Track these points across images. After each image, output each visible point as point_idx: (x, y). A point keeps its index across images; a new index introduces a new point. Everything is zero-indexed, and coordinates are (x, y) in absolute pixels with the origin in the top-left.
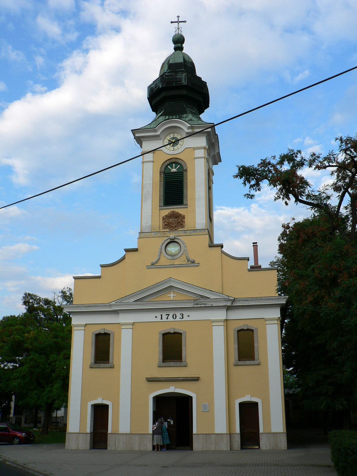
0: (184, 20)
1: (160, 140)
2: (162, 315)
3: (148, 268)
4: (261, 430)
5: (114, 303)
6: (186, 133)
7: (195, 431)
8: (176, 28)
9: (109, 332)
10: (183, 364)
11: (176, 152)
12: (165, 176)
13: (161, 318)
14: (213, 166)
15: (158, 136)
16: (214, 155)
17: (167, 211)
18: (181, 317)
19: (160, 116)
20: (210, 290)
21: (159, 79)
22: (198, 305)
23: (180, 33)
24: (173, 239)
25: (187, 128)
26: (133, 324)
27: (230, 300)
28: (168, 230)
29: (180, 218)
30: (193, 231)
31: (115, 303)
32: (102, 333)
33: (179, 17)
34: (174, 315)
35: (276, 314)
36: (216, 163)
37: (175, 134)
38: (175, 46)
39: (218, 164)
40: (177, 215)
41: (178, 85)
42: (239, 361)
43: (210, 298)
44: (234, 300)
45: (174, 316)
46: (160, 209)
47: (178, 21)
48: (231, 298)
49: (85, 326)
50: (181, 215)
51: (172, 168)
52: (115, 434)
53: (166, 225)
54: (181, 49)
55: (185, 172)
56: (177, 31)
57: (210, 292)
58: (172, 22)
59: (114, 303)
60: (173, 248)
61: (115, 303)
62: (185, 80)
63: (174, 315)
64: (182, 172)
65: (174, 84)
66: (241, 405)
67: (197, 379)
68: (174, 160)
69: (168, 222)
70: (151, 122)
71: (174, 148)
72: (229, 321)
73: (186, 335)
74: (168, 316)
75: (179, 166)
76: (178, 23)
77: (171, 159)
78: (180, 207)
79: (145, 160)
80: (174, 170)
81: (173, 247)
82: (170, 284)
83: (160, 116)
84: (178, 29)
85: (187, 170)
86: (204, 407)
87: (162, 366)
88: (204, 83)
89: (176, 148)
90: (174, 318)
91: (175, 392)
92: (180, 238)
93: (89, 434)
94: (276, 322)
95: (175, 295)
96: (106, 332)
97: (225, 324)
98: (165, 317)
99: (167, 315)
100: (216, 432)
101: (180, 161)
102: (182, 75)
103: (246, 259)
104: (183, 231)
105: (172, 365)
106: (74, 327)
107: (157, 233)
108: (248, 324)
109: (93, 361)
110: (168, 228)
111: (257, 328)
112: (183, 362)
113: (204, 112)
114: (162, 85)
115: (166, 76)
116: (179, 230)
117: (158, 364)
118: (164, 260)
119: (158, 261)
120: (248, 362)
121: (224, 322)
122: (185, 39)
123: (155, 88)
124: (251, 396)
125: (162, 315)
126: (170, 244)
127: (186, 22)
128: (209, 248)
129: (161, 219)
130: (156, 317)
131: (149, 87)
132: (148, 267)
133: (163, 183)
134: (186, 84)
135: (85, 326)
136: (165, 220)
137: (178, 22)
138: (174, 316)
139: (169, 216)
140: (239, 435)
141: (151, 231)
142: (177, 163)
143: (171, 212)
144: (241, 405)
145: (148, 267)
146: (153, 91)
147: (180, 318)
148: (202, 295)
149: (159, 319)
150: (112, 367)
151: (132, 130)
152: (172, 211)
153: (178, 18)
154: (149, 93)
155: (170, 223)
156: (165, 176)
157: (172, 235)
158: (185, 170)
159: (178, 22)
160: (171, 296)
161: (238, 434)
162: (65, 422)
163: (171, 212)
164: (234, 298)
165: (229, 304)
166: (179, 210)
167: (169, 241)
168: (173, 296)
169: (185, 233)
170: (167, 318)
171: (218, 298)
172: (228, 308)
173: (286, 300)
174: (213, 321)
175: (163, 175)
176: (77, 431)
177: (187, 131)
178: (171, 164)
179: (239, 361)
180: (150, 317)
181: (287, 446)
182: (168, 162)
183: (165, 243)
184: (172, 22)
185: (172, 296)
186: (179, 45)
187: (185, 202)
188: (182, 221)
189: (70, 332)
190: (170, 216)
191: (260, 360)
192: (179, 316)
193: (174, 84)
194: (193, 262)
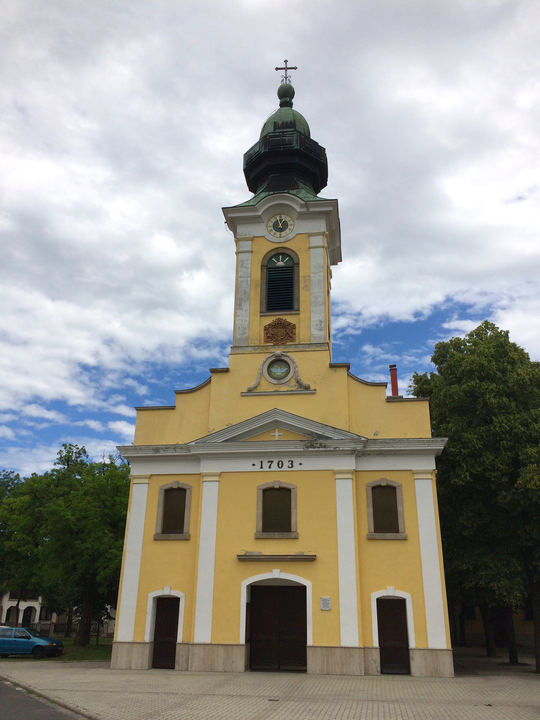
0: (293, 67)
1: (263, 223)
2: (262, 462)
3: (242, 396)
4: (412, 644)
5: (193, 443)
6: (297, 214)
7: (310, 642)
8: (283, 77)
9: (185, 487)
10: (293, 535)
11: (282, 240)
12: (269, 271)
13: (260, 467)
14: (331, 266)
15: (259, 217)
16: (333, 249)
17: (269, 320)
18: (290, 466)
19: (261, 192)
20: (332, 427)
21: (261, 141)
22: (315, 448)
23: (288, 83)
24: (279, 356)
25: (300, 205)
26: (220, 475)
27: (362, 442)
28: (272, 344)
29: (289, 328)
30: (307, 345)
31: (195, 443)
32: (174, 487)
33: (287, 61)
34: (280, 463)
35: (431, 465)
36: (334, 263)
37: (282, 215)
38: (281, 102)
39: (337, 265)
40: (285, 324)
41: (287, 149)
42: (374, 533)
43: (332, 438)
44: (367, 441)
45: (280, 464)
46: (261, 316)
47: (286, 67)
48: (363, 439)
49: (149, 478)
50: (290, 323)
51: (279, 261)
52: (187, 645)
53: (269, 337)
54: (290, 105)
55: (296, 267)
56: (284, 81)
57: (332, 429)
58: (277, 69)
59: (193, 443)
60: (279, 369)
61: (195, 443)
62: (297, 142)
63: (280, 463)
64: (292, 267)
65: (280, 148)
66: (381, 602)
67: (311, 559)
68: (281, 251)
69: (272, 333)
70: (250, 199)
71: (280, 235)
72: (359, 473)
73: (296, 492)
74: (271, 463)
75: (288, 258)
76: (286, 70)
77: (277, 248)
78: (288, 313)
79: (241, 249)
80: (281, 264)
81: (279, 367)
82: (275, 417)
83: (261, 192)
84: (286, 78)
85: (299, 264)
86: (323, 604)
87: (261, 537)
88: (322, 149)
89: (283, 234)
90: (280, 466)
91: (280, 578)
92: (288, 354)
93: (149, 645)
94: (430, 476)
95: (282, 434)
96: (181, 486)
97: (354, 478)
98: (266, 465)
99: (269, 462)
100: (344, 644)
101: (288, 252)
102: (293, 136)
103: (383, 385)
104: (294, 346)
105: (276, 537)
106: (134, 479)
107: (257, 347)
108: (388, 479)
109: (159, 530)
110: (272, 341)
111: (401, 485)
112: (292, 533)
113: (320, 192)
114: (265, 148)
115: (271, 137)
116: (287, 344)
117: (255, 534)
118: (266, 385)
119: (257, 386)
120: (388, 535)
121: (352, 473)
122: (293, 103)
123: (255, 155)
124: (395, 589)
125: (262, 462)
126: (274, 364)
127: (297, 68)
128: (330, 368)
129: (263, 328)
130: (254, 465)
131: (246, 153)
132: (243, 395)
133: (265, 280)
134: (298, 148)
135: (149, 478)
136: (267, 331)
137: (286, 69)
138: (280, 464)
139: (274, 324)
140: (379, 650)
141: (247, 346)
142: (284, 255)
143: (276, 319)
144: (381, 602)
145: (243, 395)
146: (253, 159)
147: (288, 467)
148: (321, 433)
149: (257, 468)
150: (187, 539)
151: (223, 208)
152: (278, 318)
153: (286, 63)
154: (246, 162)
155: (275, 334)
156: (269, 271)
157: (278, 351)
158: (296, 264)
159: (286, 69)
160: (275, 435)
161: (376, 648)
162: (110, 631)
163: (276, 319)
164: (368, 439)
165: (359, 447)
166: (290, 318)
167: (273, 358)
168: (279, 435)
169: (296, 347)
170: (270, 467)
171: (343, 438)
172: (359, 455)
173: (445, 443)
174: (335, 472)
175: (265, 270)
176: (130, 639)
177: (299, 210)
178: (276, 256)
179: (374, 533)
180: (245, 466)
181: (453, 672)
182: (273, 253)
183: (268, 361)
184: (277, 69)
185: (277, 434)
186: (288, 99)
187: (296, 307)
188: (291, 333)
189: (127, 487)
190: (275, 325)
191: (406, 532)
192: (286, 464)
193: (280, 148)
194: (307, 388)
